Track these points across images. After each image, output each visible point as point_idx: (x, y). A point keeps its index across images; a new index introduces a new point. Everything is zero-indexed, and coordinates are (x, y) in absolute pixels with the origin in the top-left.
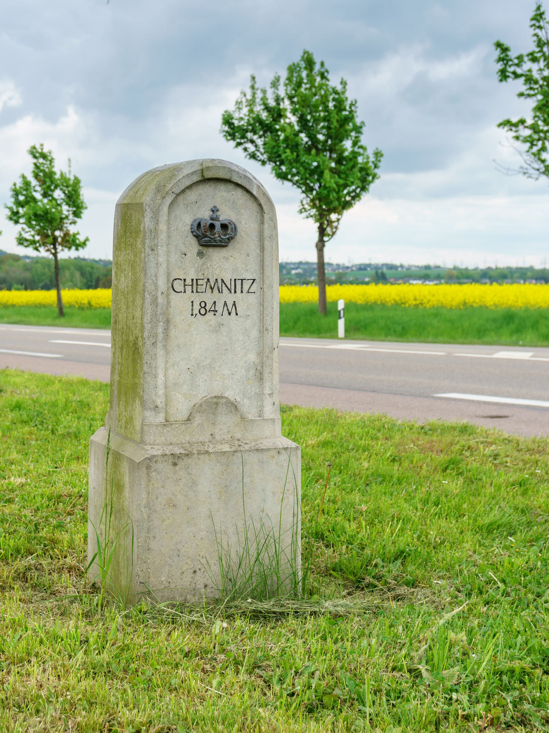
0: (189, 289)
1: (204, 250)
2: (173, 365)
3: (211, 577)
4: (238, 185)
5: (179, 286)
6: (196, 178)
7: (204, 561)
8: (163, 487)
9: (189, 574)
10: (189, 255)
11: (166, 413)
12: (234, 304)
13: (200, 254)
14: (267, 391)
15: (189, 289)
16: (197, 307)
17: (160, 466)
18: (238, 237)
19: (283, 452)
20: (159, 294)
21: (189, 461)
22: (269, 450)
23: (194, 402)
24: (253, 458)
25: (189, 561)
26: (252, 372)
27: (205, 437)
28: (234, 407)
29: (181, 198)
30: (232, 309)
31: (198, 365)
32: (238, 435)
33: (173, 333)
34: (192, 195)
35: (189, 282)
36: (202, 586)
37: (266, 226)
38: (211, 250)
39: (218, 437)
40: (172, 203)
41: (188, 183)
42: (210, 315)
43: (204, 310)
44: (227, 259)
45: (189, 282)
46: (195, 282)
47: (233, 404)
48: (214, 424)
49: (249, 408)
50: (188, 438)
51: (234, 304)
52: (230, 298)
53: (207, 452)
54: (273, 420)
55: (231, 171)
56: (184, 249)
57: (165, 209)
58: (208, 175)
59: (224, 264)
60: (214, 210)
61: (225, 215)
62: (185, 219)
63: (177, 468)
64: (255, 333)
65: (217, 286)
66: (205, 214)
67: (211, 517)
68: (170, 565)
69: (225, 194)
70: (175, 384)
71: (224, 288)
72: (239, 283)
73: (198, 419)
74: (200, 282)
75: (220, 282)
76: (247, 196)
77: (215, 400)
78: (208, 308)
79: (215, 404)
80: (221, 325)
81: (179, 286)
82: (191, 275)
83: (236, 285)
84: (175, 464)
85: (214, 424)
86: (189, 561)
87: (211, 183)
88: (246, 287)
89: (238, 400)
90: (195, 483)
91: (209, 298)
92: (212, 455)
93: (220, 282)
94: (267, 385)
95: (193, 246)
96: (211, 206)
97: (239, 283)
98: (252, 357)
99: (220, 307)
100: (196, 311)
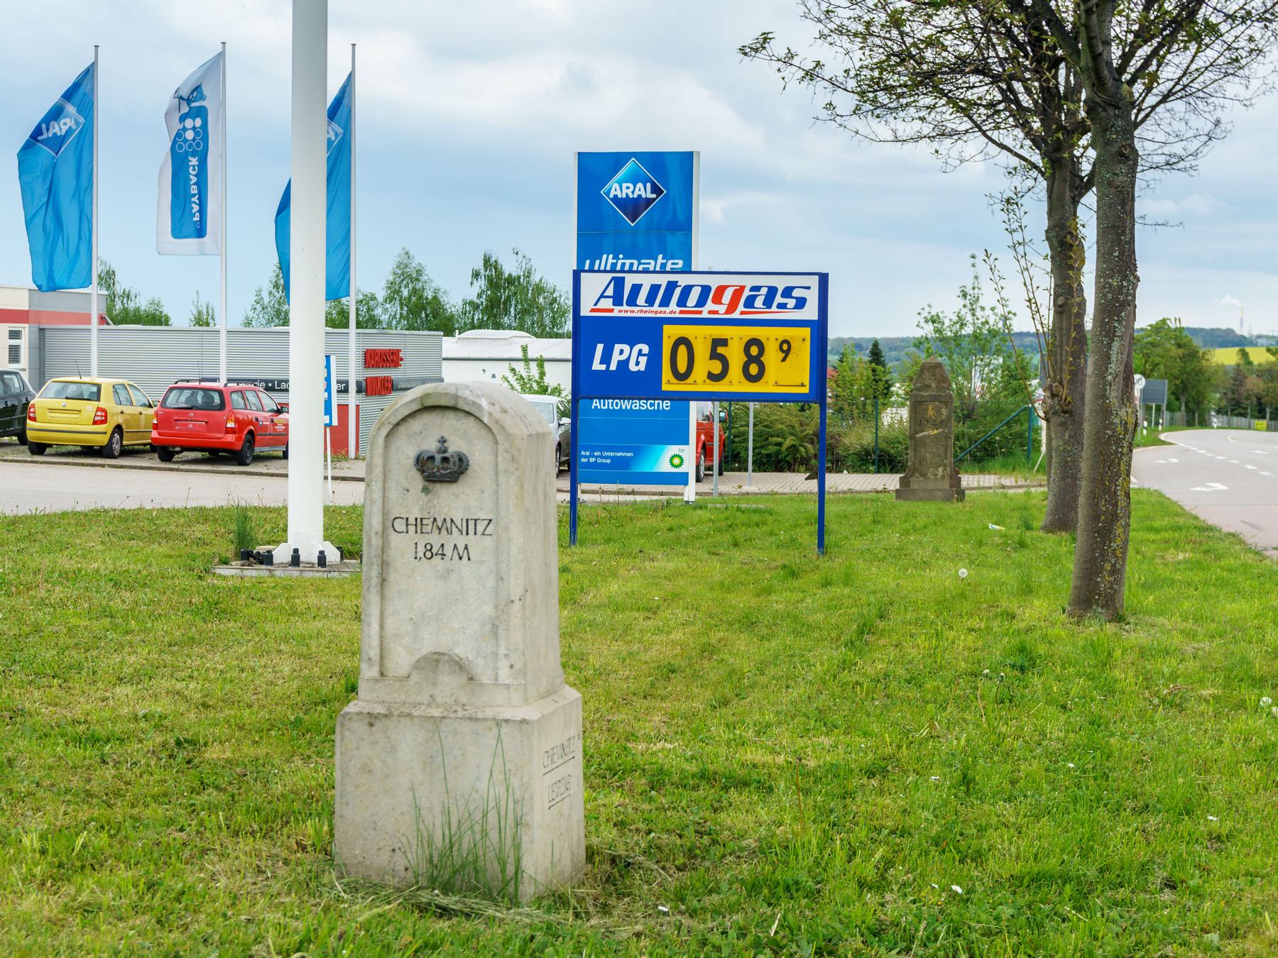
0: (412, 529)
1: (431, 486)
2: (394, 614)
3: (412, 858)
4: (469, 413)
5: (400, 525)
6: (415, 407)
7: (404, 840)
8: (357, 749)
9: (387, 851)
10: (412, 491)
11: (382, 665)
12: (466, 548)
13: (425, 490)
14: (502, 651)
15: (412, 529)
16: (421, 550)
17: (354, 725)
18: (470, 471)
19: (504, 724)
20: (373, 534)
21: (388, 722)
22: (485, 720)
23: (418, 656)
24: (466, 727)
25: (387, 837)
26: (488, 628)
27: (424, 698)
28: (459, 666)
29: (402, 428)
30: (463, 554)
31: (423, 615)
32: (464, 700)
33: (393, 577)
34: (415, 425)
35: (412, 521)
36: (402, 868)
37: (500, 458)
38: (438, 485)
39: (439, 700)
40: (387, 436)
41: (407, 412)
42: (437, 559)
43: (430, 554)
44: (457, 496)
45: (412, 521)
46: (419, 522)
47: (457, 663)
48: (434, 684)
49: (481, 668)
50: (403, 697)
51: (466, 548)
52: (461, 541)
53: (409, 715)
54: (508, 686)
55: (456, 397)
56: (406, 485)
57: (381, 440)
58: (429, 403)
59: (452, 501)
60: (443, 441)
61: (454, 447)
62: (407, 450)
63: (374, 729)
64: (491, 582)
65: (444, 526)
66: (431, 446)
67: (412, 789)
68: (366, 839)
69: (454, 422)
70: (395, 635)
71: (454, 529)
72: (471, 524)
73: (415, 678)
74: (425, 522)
75: (448, 521)
76: (479, 425)
77: (435, 657)
78: (434, 551)
79: (434, 662)
80: (449, 571)
81: (400, 525)
82: (415, 513)
83: (470, 525)
84: (371, 725)
85: (434, 684)
86: (387, 837)
87: (438, 411)
88: (480, 527)
89: (471, 658)
90: (394, 749)
91: (436, 540)
92: (416, 720)
93: (448, 521)
94: (502, 643)
95: (417, 481)
96: (438, 437)
97: (471, 524)
98: (488, 610)
99: (448, 550)
100: (420, 554)
